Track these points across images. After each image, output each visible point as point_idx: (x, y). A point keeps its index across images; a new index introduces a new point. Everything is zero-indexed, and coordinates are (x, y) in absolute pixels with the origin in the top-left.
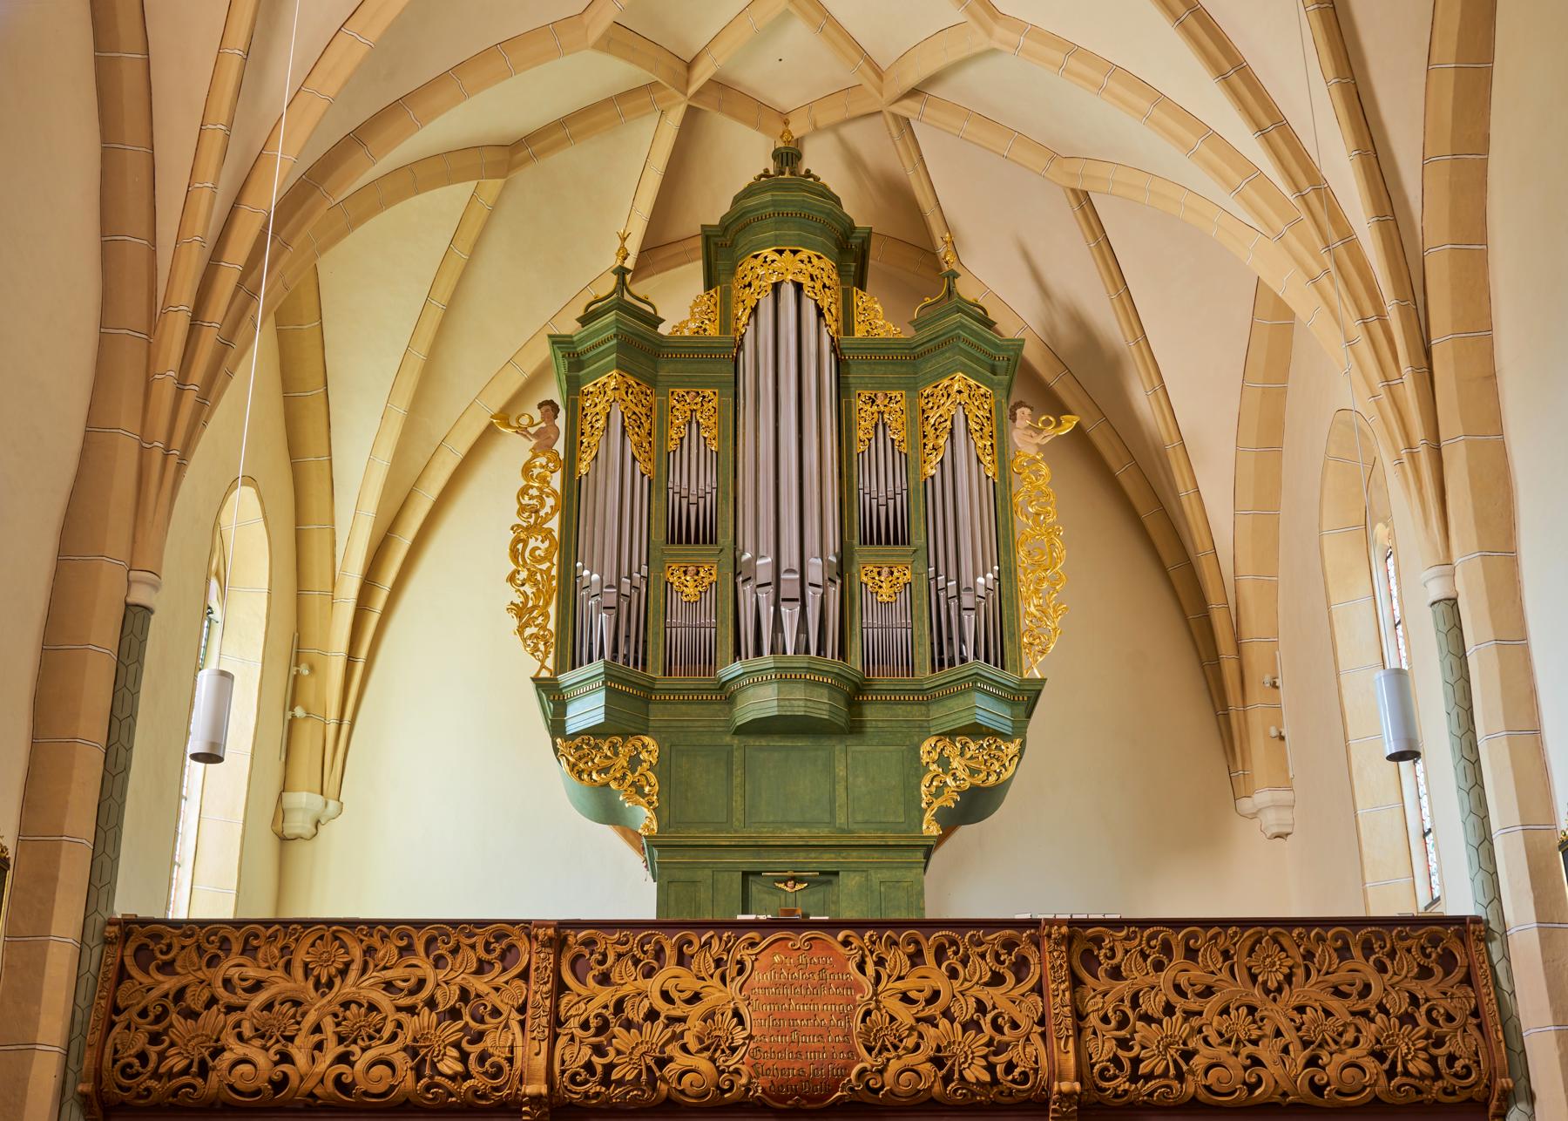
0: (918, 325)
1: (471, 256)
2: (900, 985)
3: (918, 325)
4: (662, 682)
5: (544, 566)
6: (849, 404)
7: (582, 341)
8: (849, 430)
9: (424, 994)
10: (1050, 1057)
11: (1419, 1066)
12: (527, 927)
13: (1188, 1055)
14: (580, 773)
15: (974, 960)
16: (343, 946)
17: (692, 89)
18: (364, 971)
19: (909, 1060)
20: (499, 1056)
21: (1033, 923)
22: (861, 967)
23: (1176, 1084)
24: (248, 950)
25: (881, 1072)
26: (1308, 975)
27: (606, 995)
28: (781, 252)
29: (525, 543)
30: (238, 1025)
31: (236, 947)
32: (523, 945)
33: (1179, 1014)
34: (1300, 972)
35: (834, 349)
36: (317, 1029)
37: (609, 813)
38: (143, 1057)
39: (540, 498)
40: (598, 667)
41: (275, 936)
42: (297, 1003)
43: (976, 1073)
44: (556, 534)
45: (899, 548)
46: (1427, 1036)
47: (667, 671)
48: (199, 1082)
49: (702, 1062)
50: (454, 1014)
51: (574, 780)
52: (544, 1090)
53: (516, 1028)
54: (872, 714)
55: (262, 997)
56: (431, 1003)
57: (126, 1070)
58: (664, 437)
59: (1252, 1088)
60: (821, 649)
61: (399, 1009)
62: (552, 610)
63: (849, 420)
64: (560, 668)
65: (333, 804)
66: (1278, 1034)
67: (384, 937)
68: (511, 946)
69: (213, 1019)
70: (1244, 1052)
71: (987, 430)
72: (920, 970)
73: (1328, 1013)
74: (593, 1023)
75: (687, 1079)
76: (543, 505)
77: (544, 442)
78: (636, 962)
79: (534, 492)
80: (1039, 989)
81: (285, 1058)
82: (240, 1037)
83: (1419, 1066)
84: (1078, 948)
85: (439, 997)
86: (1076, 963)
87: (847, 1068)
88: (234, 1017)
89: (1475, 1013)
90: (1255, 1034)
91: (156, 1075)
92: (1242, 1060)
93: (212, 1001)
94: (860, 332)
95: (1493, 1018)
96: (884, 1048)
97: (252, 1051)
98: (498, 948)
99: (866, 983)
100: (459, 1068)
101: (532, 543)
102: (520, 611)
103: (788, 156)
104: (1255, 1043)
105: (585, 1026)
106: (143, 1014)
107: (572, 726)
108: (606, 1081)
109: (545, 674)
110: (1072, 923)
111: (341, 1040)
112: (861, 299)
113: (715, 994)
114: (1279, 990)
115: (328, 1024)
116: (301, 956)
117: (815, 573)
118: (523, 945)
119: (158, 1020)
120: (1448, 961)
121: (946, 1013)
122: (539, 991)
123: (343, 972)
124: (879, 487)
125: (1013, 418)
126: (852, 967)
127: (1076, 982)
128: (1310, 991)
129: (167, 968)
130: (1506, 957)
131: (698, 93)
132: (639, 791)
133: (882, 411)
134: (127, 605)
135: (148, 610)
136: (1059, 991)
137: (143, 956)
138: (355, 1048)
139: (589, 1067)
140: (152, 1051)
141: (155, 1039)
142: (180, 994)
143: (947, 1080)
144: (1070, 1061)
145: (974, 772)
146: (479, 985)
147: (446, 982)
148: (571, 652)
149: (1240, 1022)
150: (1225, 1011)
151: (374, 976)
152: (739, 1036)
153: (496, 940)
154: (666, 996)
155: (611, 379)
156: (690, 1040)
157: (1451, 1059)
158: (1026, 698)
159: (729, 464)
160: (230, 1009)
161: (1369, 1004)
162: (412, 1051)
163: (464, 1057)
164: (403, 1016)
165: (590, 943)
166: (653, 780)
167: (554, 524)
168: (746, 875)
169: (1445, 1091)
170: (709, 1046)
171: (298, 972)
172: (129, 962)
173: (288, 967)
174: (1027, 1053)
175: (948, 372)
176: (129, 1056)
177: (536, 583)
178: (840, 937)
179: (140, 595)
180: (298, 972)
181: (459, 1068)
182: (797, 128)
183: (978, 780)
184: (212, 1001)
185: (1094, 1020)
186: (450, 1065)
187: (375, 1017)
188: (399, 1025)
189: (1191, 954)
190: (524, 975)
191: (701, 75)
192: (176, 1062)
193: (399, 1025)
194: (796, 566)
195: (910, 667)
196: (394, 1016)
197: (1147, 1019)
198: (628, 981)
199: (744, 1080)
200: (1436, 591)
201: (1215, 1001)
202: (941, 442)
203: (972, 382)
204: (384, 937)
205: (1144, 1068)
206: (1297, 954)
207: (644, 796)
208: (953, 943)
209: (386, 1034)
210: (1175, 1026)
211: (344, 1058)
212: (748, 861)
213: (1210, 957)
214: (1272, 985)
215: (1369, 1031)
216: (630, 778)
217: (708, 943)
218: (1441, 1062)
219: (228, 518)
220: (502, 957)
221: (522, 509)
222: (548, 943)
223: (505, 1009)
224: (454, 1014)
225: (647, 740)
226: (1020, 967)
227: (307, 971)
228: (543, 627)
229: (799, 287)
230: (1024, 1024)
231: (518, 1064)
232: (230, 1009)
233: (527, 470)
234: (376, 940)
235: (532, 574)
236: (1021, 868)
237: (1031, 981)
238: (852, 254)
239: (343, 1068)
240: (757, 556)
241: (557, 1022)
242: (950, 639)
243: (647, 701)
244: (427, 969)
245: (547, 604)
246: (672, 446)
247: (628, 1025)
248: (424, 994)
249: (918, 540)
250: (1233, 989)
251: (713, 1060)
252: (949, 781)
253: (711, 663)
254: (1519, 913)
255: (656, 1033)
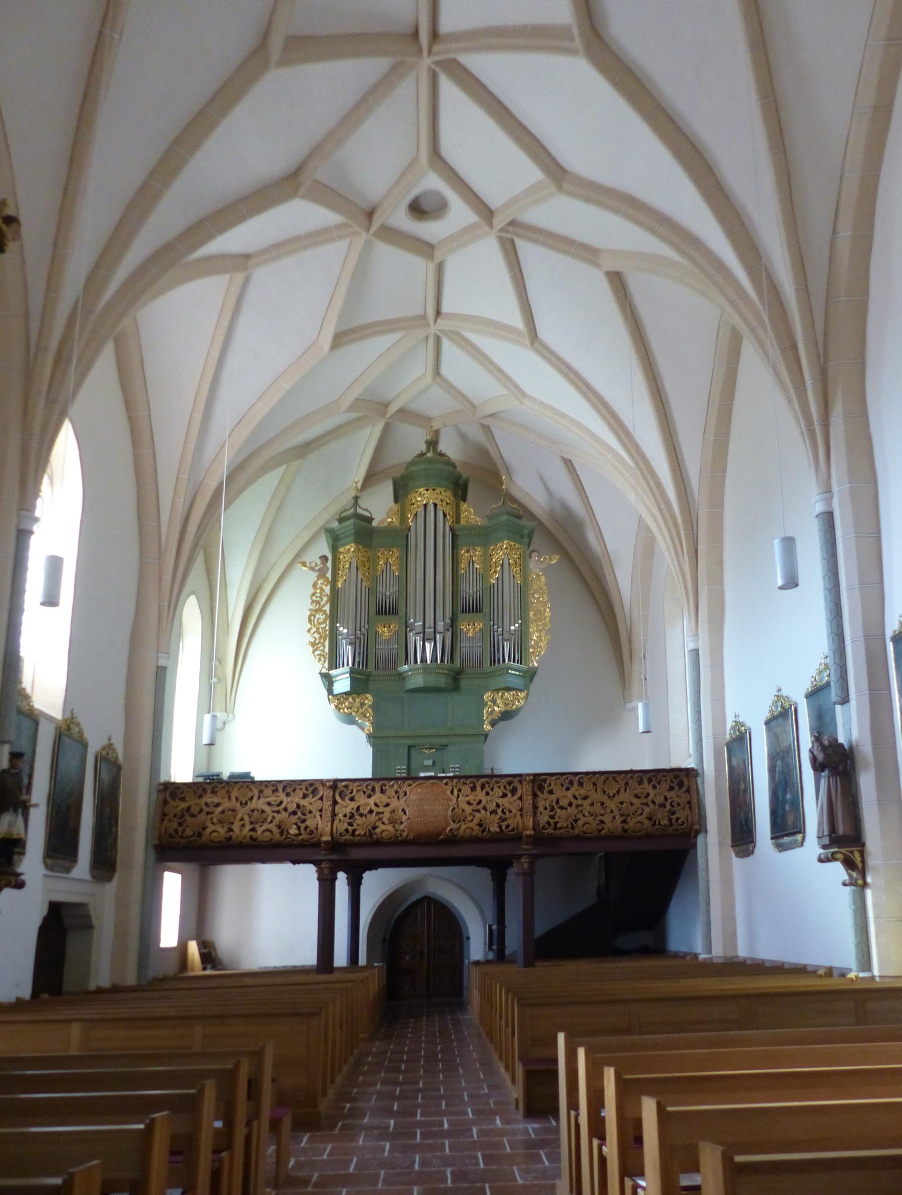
0: (490, 518)
1: (396, 842)
2: (467, 799)
3: (490, 518)
4: (375, 673)
5: (323, 626)
6: (457, 553)
7: (338, 530)
8: (457, 563)
9: (283, 806)
10: (523, 822)
11: (665, 822)
12: (322, 782)
13: (576, 821)
14: (339, 709)
15: (496, 789)
16: (250, 790)
17: (388, 416)
18: (259, 798)
19: (469, 825)
20: (312, 827)
21: (520, 775)
22: (452, 792)
23: (571, 831)
24: (214, 792)
25: (458, 829)
26: (626, 790)
27: (353, 805)
28: (427, 490)
29: (315, 616)
30: (212, 819)
31: (209, 791)
32: (321, 788)
33: (574, 806)
34: (622, 790)
35: (451, 529)
36: (242, 819)
37: (350, 721)
38: (176, 831)
39: (321, 597)
40: (346, 669)
41: (224, 787)
42: (233, 811)
43: (494, 828)
44: (328, 612)
45: (478, 614)
46: (669, 811)
47: (377, 668)
48: (198, 839)
49: (390, 828)
50: (294, 813)
51: (337, 711)
52: (330, 839)
53: (318, 817)
54: (464, 683)
55: (220, 809)
56: (285, 809)
57: (170, 836)
58: (375, 570)
59: (600, 831)
60: (442, 661)
61: (273, 812)
62: (327, 644)
63: (457, 559)
64: (330, 668)
65: (231, 716)
66: (612, 812)
67: (266, 786)
68: (316, 789)
69: (202, 816)
70: (598, 819)
71: (518, 564)
72: (475, 793)
73: (632, 804)
74: (348, 815)
75: (384, 834)
76: (322, 600)
77: (322, 573)
78: (364, 793)
79: (318, 595)
80: (521, 799)
81: (230, 830)
82: (213, 823)
83: (665, 822)
84: (536, 784)
85: (288, 807)
86: (536, 789)
87: (446, 828)
88: (210, 816)
89: (689, 803)
90: (603, 812)
91: (182, 837)
92: (597, 821)
93: (201, 811)
94: (463, 522)
95: (695, 806)
96: (459, 821)
97: (218, 828)
98: (311, 789)
99: (454, 798)
100: (297, 832)
101: (318, 616)
102: (313, 644)
103: (432, 444)
104: (602, 815)
105: (345, 816)
106: (175, 815)
107: (336, 692)
108: (353, 834)
109: (324, 671)
110: (535, 775)
111: (251, 823)
112: (464, 506)
113: (395, 803)
114: (614, 796)
115: (246, 818)
116: (234, 794)
117: (440, 625)
118: (321, 788)
119: (181, 818)
120: (681, 785)
121: (485, 809)
122: (327, 804)
123: (251, 799)
124: (469, 589)
125: (530, 557)
126: (449, 792)
127: (535, 795)
128: (626, 796)
129: (183, 799)
130: (703, 783)
131: (390, 418)
132: (365, 716)
133: (472, 557)
134: (158, 667)
135: (165, 668)
136: (528, 799)
137: (173, 796)
138: (257, 826)
139: (347, 830)
140: (180, 829)
141: (180, 824)
142: (188, 809)
143: (483, 831)
144: (531, 824)
145: (506, 705)
146: (304, 802)
147: (291, 802)
148: (334, 663)
149: (597, 808)
150: (592, 804)
151: (262, 800)
152: (404, 818)
153: (311, 787)
154: (376, 805)
155: (352, 547)
156: (385, 820)
157: (677, 819)
158: (530, 675)
159: (404, 580)
160: (208, 813)
161: (649, 800)
162: (279, 827)
163: (299, 828)
164: (275, 815)
165: (346, 787)
166: (370, 711)
167: (327, 608)
168: (409, 747)
169: (674, 830)
170: (392, 822)
171: (234, 799)
172: (169, 799)
173: (229, 798)
174: (515, 821)
175: (502, 540)
176: (171, 831)
177: (319, 633)
178: (444, 781)
179: (162, 663)
180: (234, 799)
181: (297, 832)
182: (436, 425)
183: (508, 708)
184: (201, 811)
185: (541, 809)
186: (293, 831)
187: (264, 815)
188: (274, 817)
189: (581, 784)
190: (321, 799)
191: (393, 409)
192: (189, 832)
193: (274, 817)
194: (432, 625)
195: (481, 664)
196: (271, 814)
197: (562, 808)
198: (361, 799)
199: (406, 833)
200: (691, 646)
201: (589, 801)
202: (498, 569)
203: (512, 543)
204: (266, 786)
205: (559, 825)
206: (622, 784)
207: (366, 717)
208: (488, 783)
209: (269, 820)
210: (572, 810)
211: (253, 830)
212: (410, 742)
213: (588, 786)
214: (611, 794)
215: (647, 810)
216: (361, 711)
217: (393, 785)
218: (674, 821)
219: (337, 883)
220: (312, 792)
221: (313, 602)
222: (331, 787)
223: (314, 811)
224: (294, 813)
225: (368, 695)
226: (514, 791)
227: (237, 799)
228: (323, 651)
229: (435, 505)
230: (514, 811)
231: (320, 830)
232: (208, 813)
233: (315, 585)
234: (263, 787)
235: (318, 629)
236: (518, 754)
237: (517, 796)
238: (460, 490)
239: (253, 833)
240: (415, 621)
241: (334, 815)
242: (498, 650)
243: (367, 680)
244: (283, 797)
245: (324, 641)
246: (379, 573)
247: (361, 815)
248: (283, 806)
249: (486, 610)
250: (598, 796)
251: (394, 827)
252: (496, 708)
253: (395, 664)
254: (709, 768)
255: (373, 818)
